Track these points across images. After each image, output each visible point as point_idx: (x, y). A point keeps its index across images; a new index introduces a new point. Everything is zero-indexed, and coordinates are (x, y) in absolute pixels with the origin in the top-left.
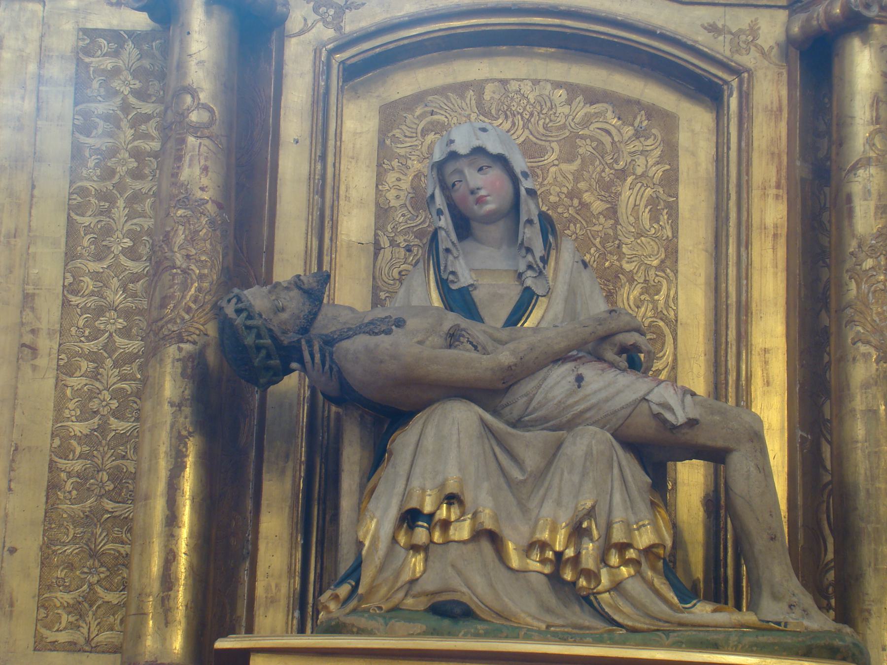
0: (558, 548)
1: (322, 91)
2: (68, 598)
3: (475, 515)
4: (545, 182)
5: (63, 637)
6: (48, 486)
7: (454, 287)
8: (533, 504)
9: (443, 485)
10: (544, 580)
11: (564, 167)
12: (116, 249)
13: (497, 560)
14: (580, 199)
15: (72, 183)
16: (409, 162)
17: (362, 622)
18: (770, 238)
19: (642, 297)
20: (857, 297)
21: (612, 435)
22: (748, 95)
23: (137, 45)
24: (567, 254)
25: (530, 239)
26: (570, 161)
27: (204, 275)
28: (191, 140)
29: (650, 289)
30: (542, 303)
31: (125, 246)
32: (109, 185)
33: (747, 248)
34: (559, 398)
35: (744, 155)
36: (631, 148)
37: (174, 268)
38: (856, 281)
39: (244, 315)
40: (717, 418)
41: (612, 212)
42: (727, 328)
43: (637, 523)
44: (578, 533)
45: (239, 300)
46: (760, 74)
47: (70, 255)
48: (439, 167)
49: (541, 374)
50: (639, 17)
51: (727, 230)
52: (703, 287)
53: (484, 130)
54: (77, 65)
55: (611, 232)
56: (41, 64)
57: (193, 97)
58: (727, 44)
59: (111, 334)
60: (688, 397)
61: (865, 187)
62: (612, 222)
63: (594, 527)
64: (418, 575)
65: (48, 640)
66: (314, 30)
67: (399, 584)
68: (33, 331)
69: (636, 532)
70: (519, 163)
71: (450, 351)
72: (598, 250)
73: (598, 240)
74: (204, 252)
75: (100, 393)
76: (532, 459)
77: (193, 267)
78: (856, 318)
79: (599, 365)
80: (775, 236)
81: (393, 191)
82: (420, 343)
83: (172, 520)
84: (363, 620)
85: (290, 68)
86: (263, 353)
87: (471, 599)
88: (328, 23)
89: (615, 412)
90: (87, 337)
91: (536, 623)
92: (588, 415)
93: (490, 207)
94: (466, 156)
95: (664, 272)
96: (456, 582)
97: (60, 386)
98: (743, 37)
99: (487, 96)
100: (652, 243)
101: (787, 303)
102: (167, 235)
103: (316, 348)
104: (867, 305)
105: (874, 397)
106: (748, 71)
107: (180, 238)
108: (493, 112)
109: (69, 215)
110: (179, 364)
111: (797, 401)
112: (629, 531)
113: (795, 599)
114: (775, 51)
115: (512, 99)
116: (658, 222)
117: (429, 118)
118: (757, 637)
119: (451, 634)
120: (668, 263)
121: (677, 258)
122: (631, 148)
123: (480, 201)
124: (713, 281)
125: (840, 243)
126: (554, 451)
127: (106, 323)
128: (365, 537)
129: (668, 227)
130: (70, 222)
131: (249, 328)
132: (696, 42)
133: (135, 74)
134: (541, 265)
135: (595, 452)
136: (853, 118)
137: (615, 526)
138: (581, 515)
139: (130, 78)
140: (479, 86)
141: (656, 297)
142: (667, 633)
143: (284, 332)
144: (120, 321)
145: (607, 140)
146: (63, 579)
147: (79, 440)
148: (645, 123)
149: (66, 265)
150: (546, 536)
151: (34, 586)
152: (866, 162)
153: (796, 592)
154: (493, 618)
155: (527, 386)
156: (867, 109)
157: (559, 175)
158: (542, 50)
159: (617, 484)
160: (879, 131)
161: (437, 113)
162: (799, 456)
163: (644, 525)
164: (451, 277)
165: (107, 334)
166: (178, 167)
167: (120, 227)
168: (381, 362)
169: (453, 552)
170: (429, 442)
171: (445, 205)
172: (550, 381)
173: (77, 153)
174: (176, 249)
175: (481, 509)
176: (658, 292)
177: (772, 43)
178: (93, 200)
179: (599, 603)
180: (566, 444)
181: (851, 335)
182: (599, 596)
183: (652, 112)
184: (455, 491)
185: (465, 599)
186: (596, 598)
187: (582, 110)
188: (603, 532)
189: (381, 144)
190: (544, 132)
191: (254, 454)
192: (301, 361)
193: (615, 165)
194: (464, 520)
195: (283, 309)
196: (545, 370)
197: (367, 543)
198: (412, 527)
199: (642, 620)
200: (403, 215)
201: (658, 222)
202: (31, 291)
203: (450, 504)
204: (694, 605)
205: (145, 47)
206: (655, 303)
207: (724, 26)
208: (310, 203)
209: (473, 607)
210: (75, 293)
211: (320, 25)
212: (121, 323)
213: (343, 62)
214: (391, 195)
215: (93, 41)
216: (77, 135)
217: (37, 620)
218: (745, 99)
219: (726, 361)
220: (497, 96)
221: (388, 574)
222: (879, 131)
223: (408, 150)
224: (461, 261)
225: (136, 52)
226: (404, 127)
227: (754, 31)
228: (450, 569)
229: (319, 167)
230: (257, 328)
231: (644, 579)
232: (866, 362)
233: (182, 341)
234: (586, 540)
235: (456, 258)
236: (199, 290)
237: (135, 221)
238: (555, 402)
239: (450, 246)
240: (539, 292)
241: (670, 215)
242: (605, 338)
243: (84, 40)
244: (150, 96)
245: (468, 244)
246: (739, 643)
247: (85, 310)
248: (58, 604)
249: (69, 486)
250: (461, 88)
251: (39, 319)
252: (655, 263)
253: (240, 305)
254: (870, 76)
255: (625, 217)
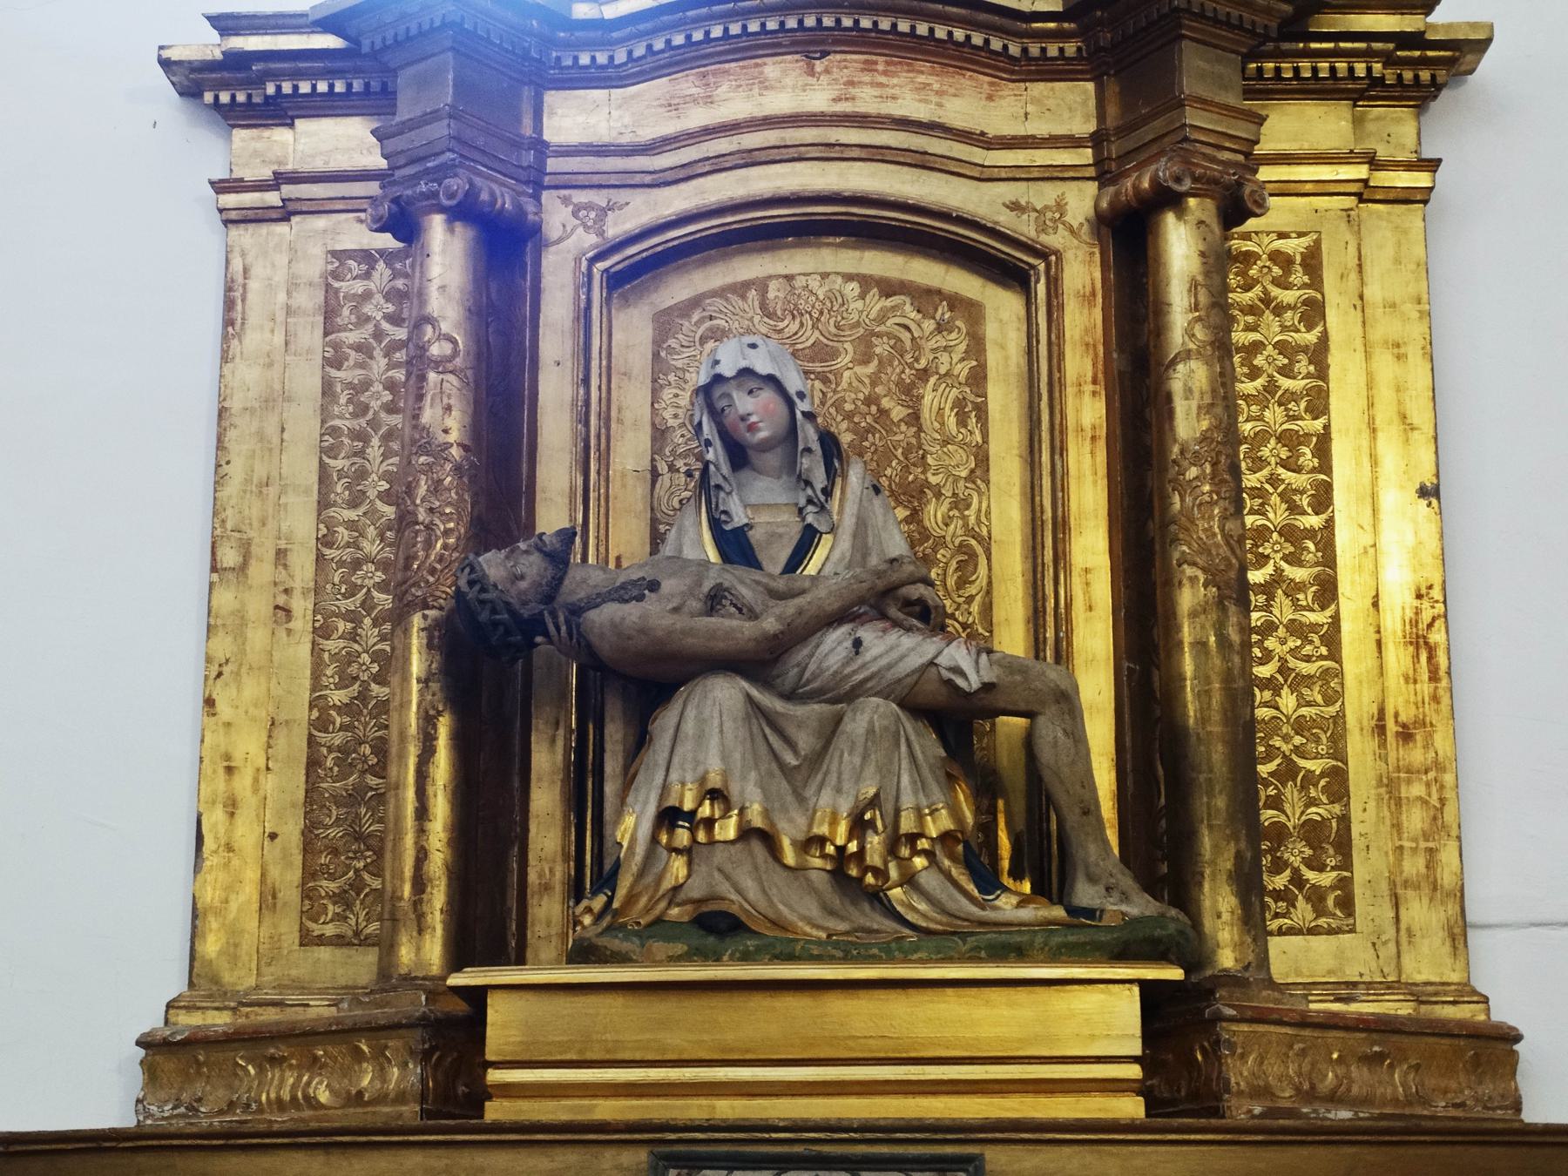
0: (840, 841)
1: (582, 305)
2: (332, 886)
3: (742, 811)
4: (839, 389)
5: (330, 930)
6: (308, 763)
7: (728, 527)
8: (809, 792)
9: (702, 780)
10: (825, 876)
11: (860, 370)
12: (372, 494)
13: (770, 860)
14: (878, 406)
15: (323, 422)
16: (687, 375)
17: (615, 944)
18: (1088, 441)
19: (951, 513)
20: (1181, 512)
21: (898, 705)
22: (1056, 280)
23: (389, 264)
24: (855, 475)
25: (809, 470)
26: (865, 361)
27: (450, 529)
28: (432, 376)
29: (960, 504)
30: (827, 541)
31: (382, 489)
32: (363, 422)
33: (1062, 455)
34: (835, 667)
35: (1055, 348)
36: (932, 344)
37: (417, 523)
38: (1180, 494)
39: (477, 587)
40: (1018, 678)
41: (915, 418)
42: (1043, 547)
43: (929, 807)
44: (859, 826)
45: (473, 570)
46: (1069, 256)
47: (323, 504)
48: (706, 391)
49: (814, 640)
50: (933, 199)
51: (1040, 436)
52: (1018, 498)
53: (753, 346)
54: (327, 292)
55: (914, 441)
56: (289, 293)
57: (434, 328)
58: (1032, 223)
59: (369, 590)
60: (984, 657)
61: (1185, 385)
62: (915, 429)
63: (878, 817)
64: (681, 881)
65: (315, 934)
66: (574, 237)
67: (660, 893)
68: (286, 591)
69: (929, 818)
70: (793, 383)
71: (709, 619)
72: (900, 462)
73: (900, 450)
74: (449, 504)
75: (359, 656)
76: (806, 741)
77: (437, 521)
78: (1181, 536)
79: (881, 625)
80: (1093, 438)
81: (669, 409)
82: (676, 610)
83: (422, 813)
84: (617, 941)
85: (548, 281)
86: (501, 629)
87: (741, 906)
88: (589, 228)
89: (899, 681)
90: (343, 595)
91: (815, 932)
92: (869, 685)
93: (763, 434)
94: (733, 378)
95: (974, 483)
96: (725, 888)
97: (316, 650)
98: (1049, 215)
99: (771, 295)
100: (960, 451)
101: (1110, 515)
102: (409, 485)
103: (561, 619)
104: (1192, 521)
105: (1203, 627)
106: (1057, 253)
107: (422, 490)
108: (779, 313)
109: (321, 458)
110: (423, 634)
111: (1123, 628)
112: (920, 817)
113: (1113, 881)
114: (1086, 228)
115: (799, 296)
116: (965, 426)
117: (708, 324)
118: (1066, 936)
119: (717, 959)
120: (978, 473)
121: (988, 465)
122: (932, 344)
123: (752, 428)
124: (1029, 490)
125: (1163, 451)
126: (830, 731)
127: (363, 578)
128: (623, 836)
129: (977, 432)
130: (323, 466)
131: (482, 602)
132: (996, 223)
133: (387, 297)
134: (822, 498)
135: (877, 729)
136: (1170, 305)
137: (903, 814)
138: (862, 805)
139: (382, 301)
140: (762, 285)
141: (966, 513)
142: (964, 936)
143: (524, 603)
144: (379, 574)
145: (906, 336)
146: (328, 866)
147: (339, 709)
148: (947, 316)
149: (319, 515)
150: (824, 830)
151: (295, 875)
152: (1187, 355)
153: (1114, 871)
154: (767, 928)
155: (801, 654)
156: (1185, 294)
157: (854, 380)
158: (831, 240)
159: (905, 764)
160: (1199, 319)
161: (716, 318)
162: (1126, 690)
163: (937, 810)
164: (723, 517)
165: (365, 590)
166: (420, 408)
167: (375, 469)
168: (629, 638)
169: (720, 855)
170: (689, 727)
171: (715, 432)
172: (824, 648)
173: (328, 389)
174: (418, 502)
175: (747, 804)
176: (968, 507)
177: (1081, 219)
178: (346, 441)
179: (889, 901)
180: (846, 719)
181: (1176, 555)
182: (889, 893)
183: (956, 302)
184: (717, 786)
185: (734, 909)
186: (886, 895)
187: (876, 303)
188: (889, 820)
189: (656, 356)
190: (833, 330)
191: (518, 724)
192: (546, 634)
193: (916, 365)
194: (731, 817)
195: (522, 577)
196: (819, 634)
197: (625, 844)
198: (672, 827)
199: (938, 917)
200: (683, 436)
201: (965, 426)
202: (283, 547)
203: (712, 800)
204: (999, 896)
205: (398, 266)
206: (965, 518)
207: (1028, 203)
208: (575, 433)
209: (743, 918)
210: (329, 545)
211: (580, 230)
212: (379, 576)
213: (606, 270)
214: (667, 414)
215: (342, 264)
216: (328, 369)
217: (302, 912)
218: (1054, 285)
219: (1043, 585)
220: (781, 295)
221: (649, 879)
222: (1199, 319)
223: (686, 361)
224: (735, 496)
225: (388, 272)
226: (680, 336)
227: (1060, 206)
228: (716, 874)
229: (582, 391)
230: (491, 602)
231: (941, 870)
232: (1192, 587)
233: (426, 606)
234: (870, 832)
235: (729, 494)
236: (445, 547)
237: (391, 461)
238: (832, 670)
239: (720, 481)
240: (822, 528)
241: (979, 418)
242: (890, 591)
243: (332, 263)
244: (403, 320)
245: (745, 474)
246: (1046, 945)
247: (341, 564)
248: (323, 894)
249: (329, 763)
250: (741, 289)
251: (292, 577)
252: (964, 474)
253: (473, 576)
254: (1187, 257)
255: (928, 422)
